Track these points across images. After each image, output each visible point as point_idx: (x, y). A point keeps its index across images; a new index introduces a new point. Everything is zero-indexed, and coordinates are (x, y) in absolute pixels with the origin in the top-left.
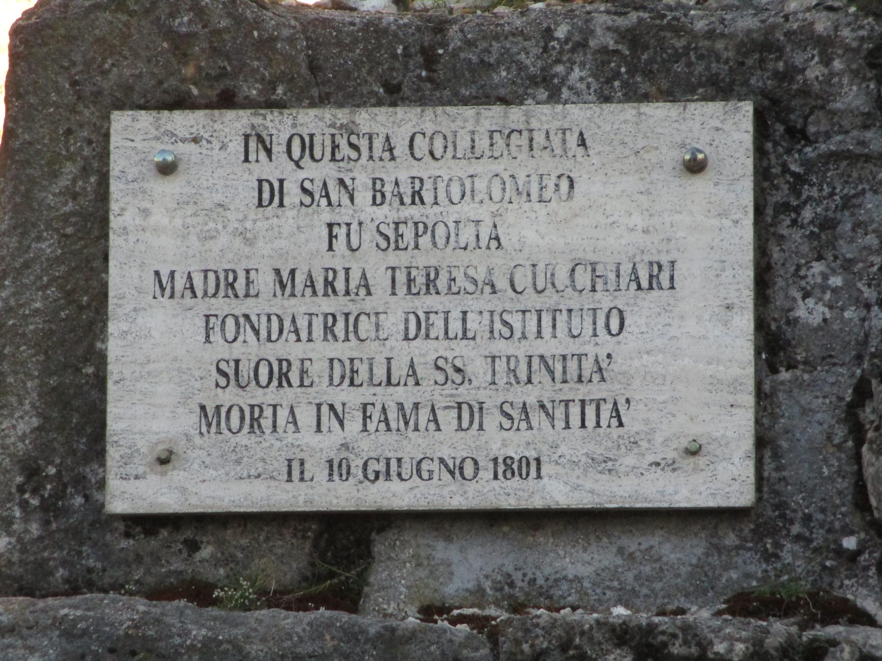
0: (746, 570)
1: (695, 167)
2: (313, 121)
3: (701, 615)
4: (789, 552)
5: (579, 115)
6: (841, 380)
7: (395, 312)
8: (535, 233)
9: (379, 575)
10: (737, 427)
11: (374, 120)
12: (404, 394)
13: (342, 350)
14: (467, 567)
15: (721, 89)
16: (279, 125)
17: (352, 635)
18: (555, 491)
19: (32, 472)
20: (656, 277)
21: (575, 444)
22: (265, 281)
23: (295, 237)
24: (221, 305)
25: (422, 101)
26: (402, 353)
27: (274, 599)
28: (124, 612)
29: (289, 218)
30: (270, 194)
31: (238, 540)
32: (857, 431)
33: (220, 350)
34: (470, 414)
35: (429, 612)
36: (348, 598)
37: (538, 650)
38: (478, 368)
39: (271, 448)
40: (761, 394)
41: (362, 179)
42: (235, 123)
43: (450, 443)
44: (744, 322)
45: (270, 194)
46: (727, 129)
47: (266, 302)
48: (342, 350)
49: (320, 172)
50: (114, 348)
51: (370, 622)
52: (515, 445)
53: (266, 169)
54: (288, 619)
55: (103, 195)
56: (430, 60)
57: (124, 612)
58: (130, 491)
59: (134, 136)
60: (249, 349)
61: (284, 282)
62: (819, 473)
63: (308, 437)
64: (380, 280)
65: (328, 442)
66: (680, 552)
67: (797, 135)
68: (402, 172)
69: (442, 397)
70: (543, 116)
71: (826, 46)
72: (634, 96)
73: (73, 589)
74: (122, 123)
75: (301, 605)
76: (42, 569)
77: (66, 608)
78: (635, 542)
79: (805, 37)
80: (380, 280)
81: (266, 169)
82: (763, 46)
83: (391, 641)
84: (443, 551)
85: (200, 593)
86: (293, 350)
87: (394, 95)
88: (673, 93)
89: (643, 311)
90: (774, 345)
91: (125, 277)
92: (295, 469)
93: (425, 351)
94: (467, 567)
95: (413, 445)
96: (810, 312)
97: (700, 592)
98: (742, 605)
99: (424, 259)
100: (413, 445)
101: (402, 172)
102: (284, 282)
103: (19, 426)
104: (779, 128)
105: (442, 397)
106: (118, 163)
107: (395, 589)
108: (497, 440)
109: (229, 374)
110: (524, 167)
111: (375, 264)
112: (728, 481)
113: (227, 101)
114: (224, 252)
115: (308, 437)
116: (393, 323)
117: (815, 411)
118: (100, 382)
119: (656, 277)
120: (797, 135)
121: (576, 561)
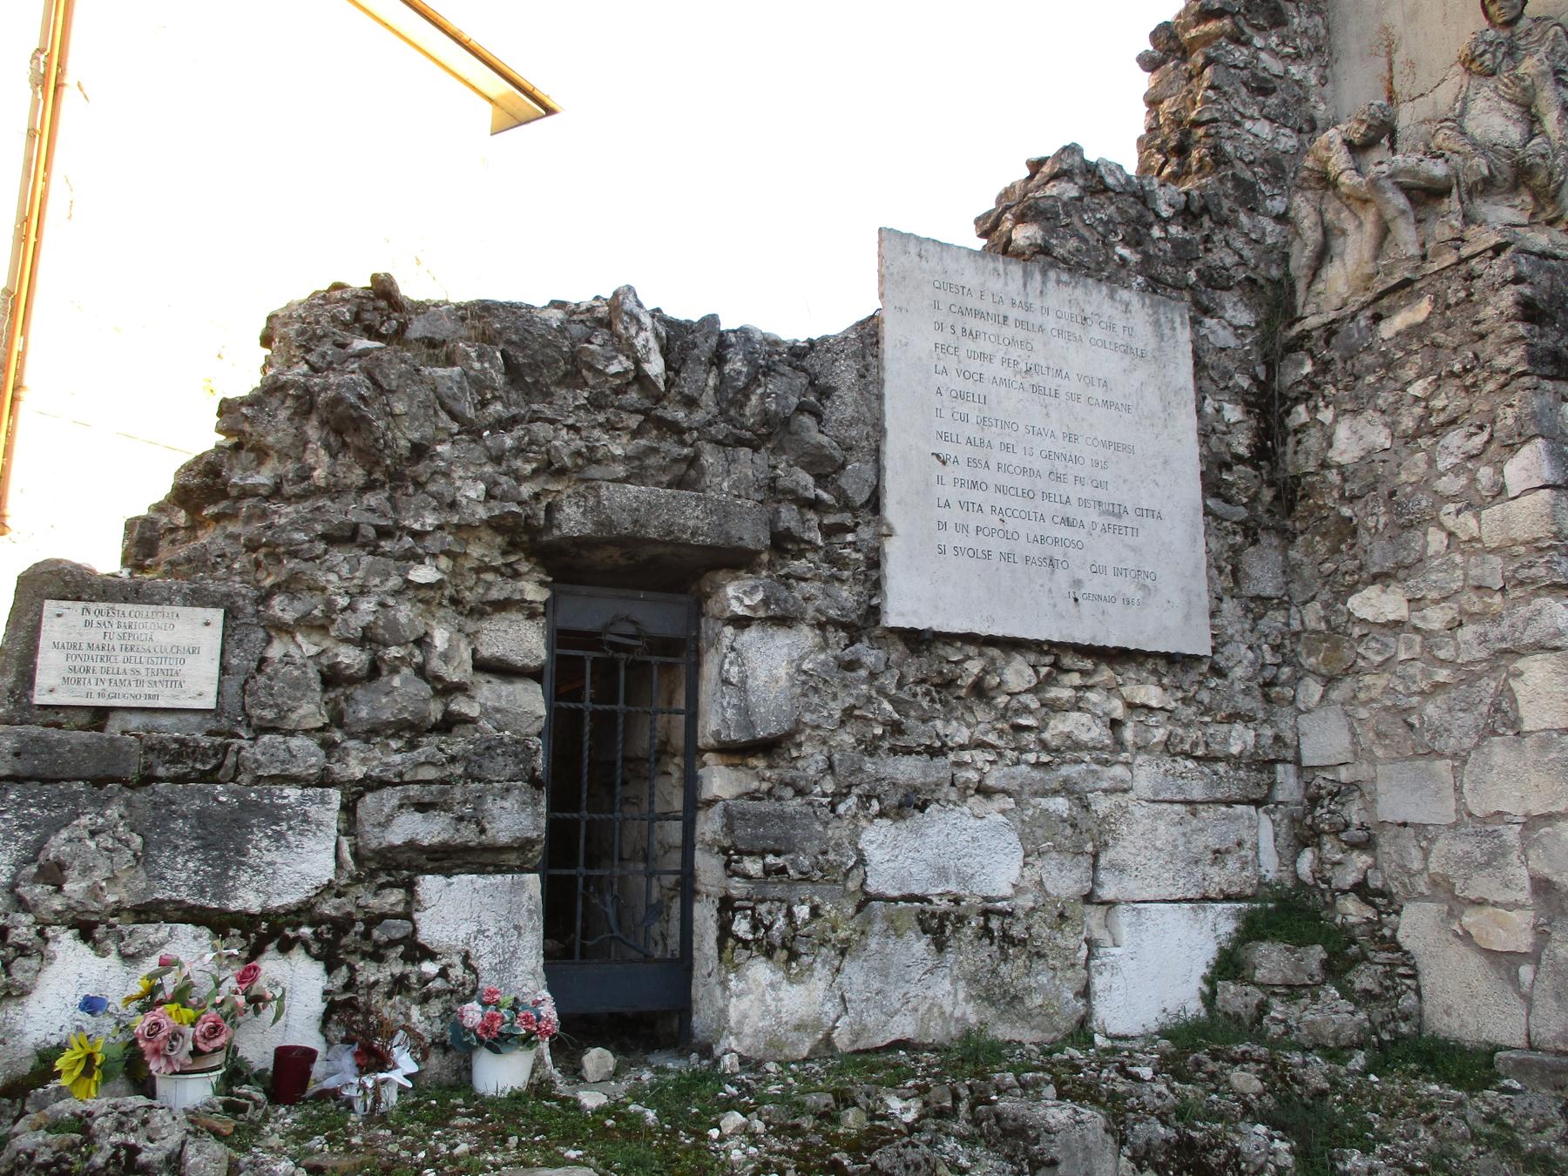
0: (212, 725)
1: (207, 624)
2: (102, 606)
3: (198, 735)
4: (224, 720)
5: (177, 609)
6: (241, 679)
7: (121, 656)
8: (163, 638)
9: (110, 722)
10: (213, 689)
11: (117, 606)
12: (122, 677)
13: (105, 665)
14: (135, 722)
15: (215, 605)
16: (93, 606)
17: (100, 738)
18: (162, 703)
19: (12, 692)
20: (194, 651)
21: (168, 691)
22: (85, 646)
23: (95, 635)
24: (71, 652)
25: (134, 603)
26: (122, 666)
27: (80, 729)
28: (35, 730)
29: (93, 630)
30: (88, 624)
31: (70, 712)
32: (244, 691)
33: (70, 663)
34: (139, 683)
35: (123, 733)
36: (101, 729)
37: (1522, 189)
38: (143, 671)
39: (83, 689)
40: (220, 681)
41: (115, 621)
42: (81, 604)
43: (134, 690)
44: (217, 663)
45: (88, 624)
46: (217, 616)
47: (85, 651)
48: (105, 665)
49: (101, 619)
50: (39, 661)
51: (106, 735)
52: (152, 691)
53: (88, 617)
54: (83, 734)
55: (40, 621)
56: (137, 592)
57: (35, 730)
58: (40, 698)
59: (50, 606)
60: (78, 663)
61: (90, 646)
62: (233, 700)
63: (93, 686)
64: (117, 647)
65: (99, 688)
66: (194, 720)
67: (235, 618)
68: (127, 620)
69: (132, 678)
70: (167, 609)
71: (244, 597)
72: (192, 605)
73: (21, 723)
74: (47, 603)
75: (809, 542)
76: (13, 717)
77: (19, 729)
78: (182, 717)
79: (239, 594)
80: (117, 647)
81: (88, 617)
82: (228, 595)
83: (112, 740)
84: (129, 717)
85: (59, 726)
86: (91, 664)
87: (126, 600)
88: (203, 605)
89: (190, 659)
90: (224, 669)
91: (44, 642)
92: (89, 695)
93: (128, 666)
94: (135, 722)
95: (123, 690)
96: (234, 661)
97: (199, 729)
98: (210, 733)
99: (131, 643)
100: (123, 690)
101: (127, 620)
102: (90, 646)
103: (9, 680)
104: (231, 615)
105: (132, 678)
106: (45, 613)
107: (114, 727)
108: (147, 690)
109: (73, 669)
110: (161, 622)
111: (116, 643)
112: (209, 702)
113: (79, 599)
114: (74, 638)
115: (93, 686)
116: (120, 658)
117: (233, 686)
118: (34, 670)
119: (194, 651)
120: (235, 618)
121: (166, 721)
